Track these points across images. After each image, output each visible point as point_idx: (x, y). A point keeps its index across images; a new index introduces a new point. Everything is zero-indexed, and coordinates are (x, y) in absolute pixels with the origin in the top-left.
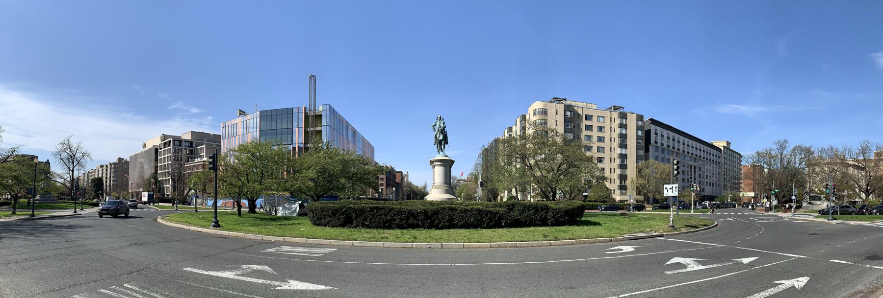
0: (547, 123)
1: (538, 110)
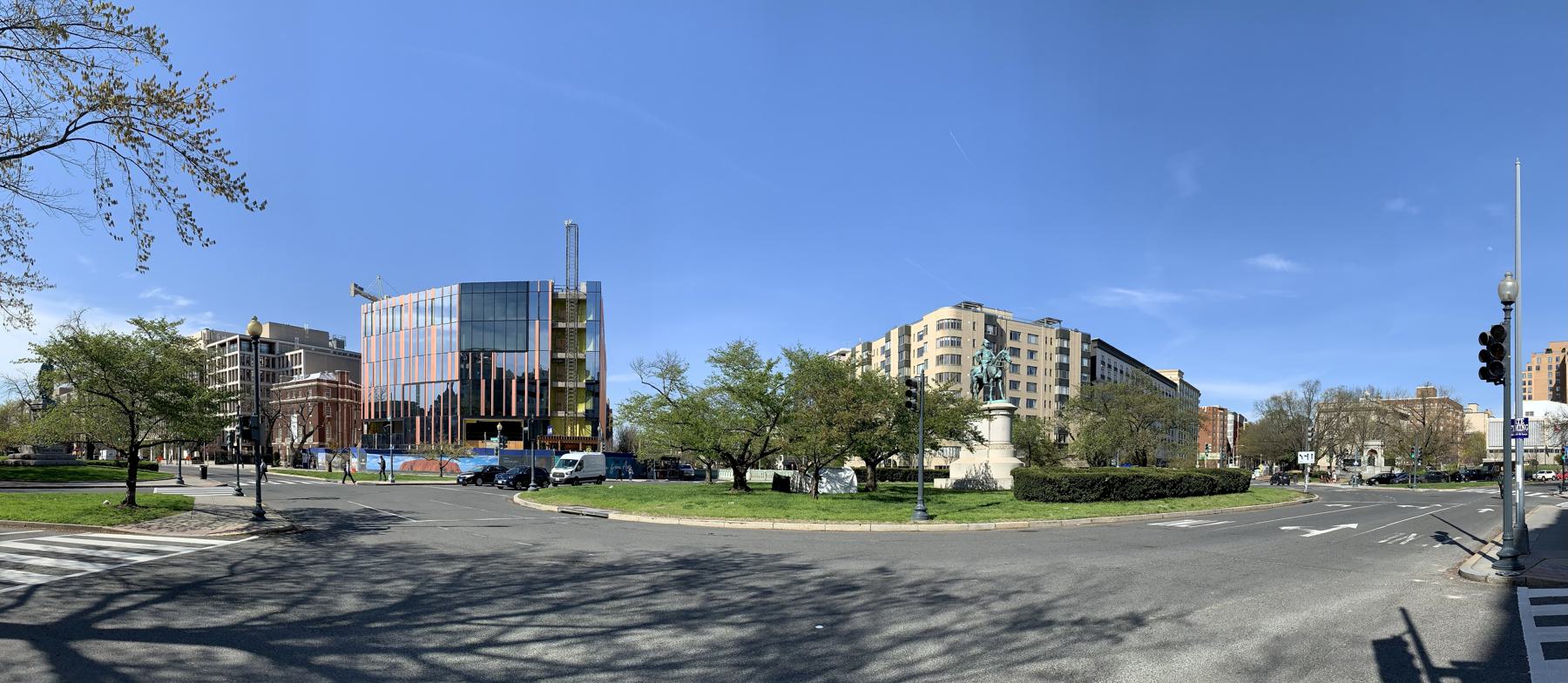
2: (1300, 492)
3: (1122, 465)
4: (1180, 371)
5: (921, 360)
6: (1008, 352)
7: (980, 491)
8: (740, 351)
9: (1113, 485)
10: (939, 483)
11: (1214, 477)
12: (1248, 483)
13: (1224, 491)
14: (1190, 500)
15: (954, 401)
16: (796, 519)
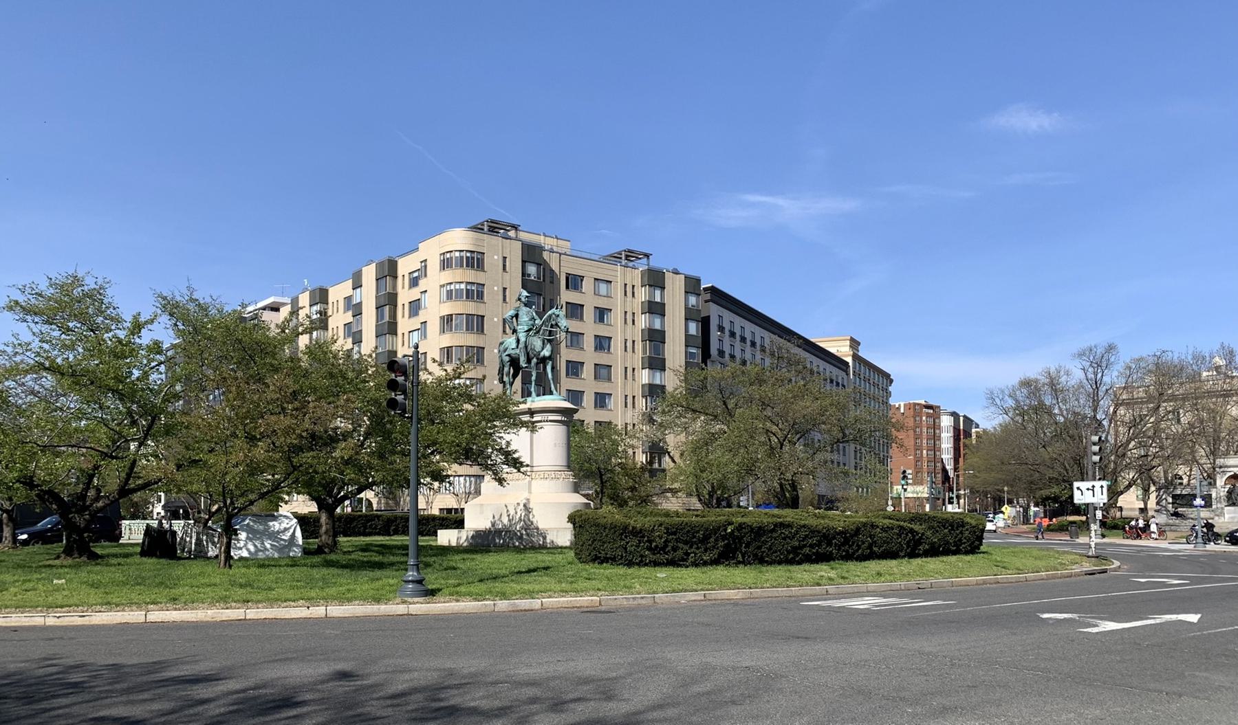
0: (482, 292)
1: (457, 254)
2: (1080, 555)
3: (758, 506)
4: (852, 340)
5: (415, 323)
6: (562, 313)
7: (518, 550)
8: (77, 292)
9: (740, 539)
10: (446, 537)
11: (916, 527)
12: (980, 538)
13: (933, 552)
14: (873, 566)
15: (470, 398)
16: (189, 603)
